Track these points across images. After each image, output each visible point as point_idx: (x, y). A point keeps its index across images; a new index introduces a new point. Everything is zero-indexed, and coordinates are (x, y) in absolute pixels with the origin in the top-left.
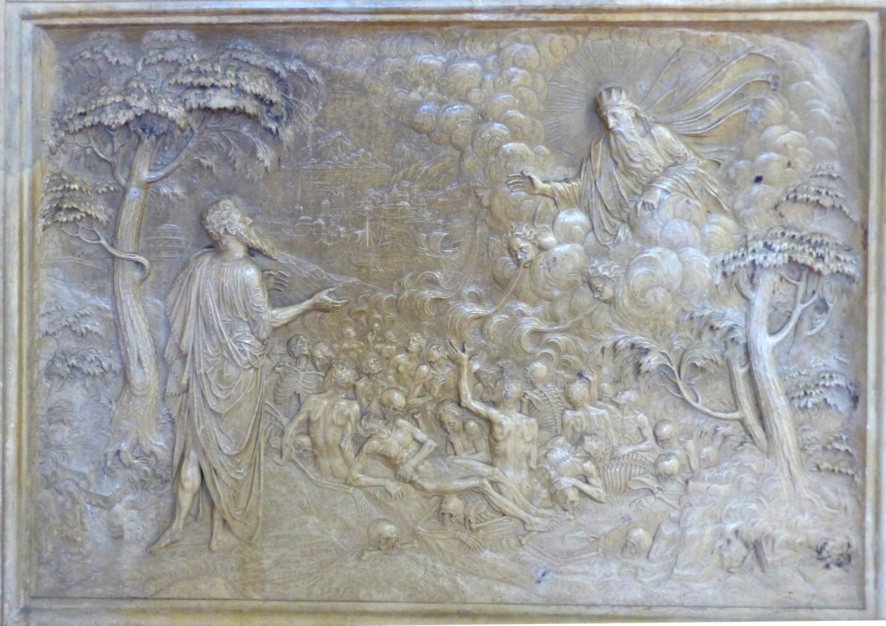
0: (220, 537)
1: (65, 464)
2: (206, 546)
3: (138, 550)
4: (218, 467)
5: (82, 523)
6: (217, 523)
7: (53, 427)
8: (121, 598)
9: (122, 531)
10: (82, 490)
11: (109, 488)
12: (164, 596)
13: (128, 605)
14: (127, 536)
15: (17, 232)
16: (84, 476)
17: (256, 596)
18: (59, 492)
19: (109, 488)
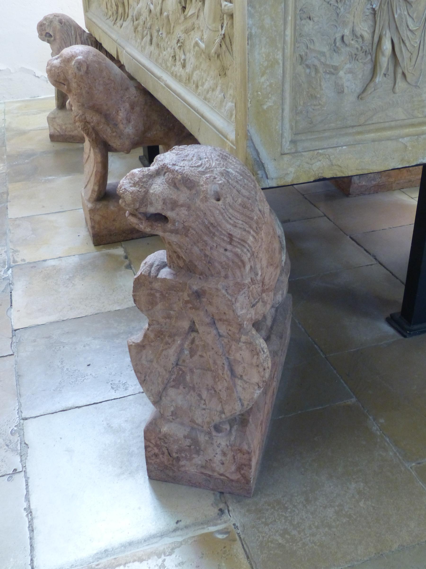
0: (400, 84)
1: (312, 47)
2: (391, 91)
3: (352, 98)
4: (405, 38)
5: (320, 85)
6: (399, 76)
7: (303, 22)
8: (346, 127)
9: (343, 88)
10: (322, 63)
11: (336, 60)
12: (370, 122)
13: (351, 130)
14: (346, 91)
15: (108, 60)
16: (323, 54)
17: (420, 116)
18: (308, 66)
19: (336, 60)
